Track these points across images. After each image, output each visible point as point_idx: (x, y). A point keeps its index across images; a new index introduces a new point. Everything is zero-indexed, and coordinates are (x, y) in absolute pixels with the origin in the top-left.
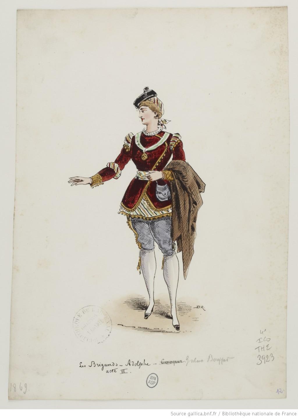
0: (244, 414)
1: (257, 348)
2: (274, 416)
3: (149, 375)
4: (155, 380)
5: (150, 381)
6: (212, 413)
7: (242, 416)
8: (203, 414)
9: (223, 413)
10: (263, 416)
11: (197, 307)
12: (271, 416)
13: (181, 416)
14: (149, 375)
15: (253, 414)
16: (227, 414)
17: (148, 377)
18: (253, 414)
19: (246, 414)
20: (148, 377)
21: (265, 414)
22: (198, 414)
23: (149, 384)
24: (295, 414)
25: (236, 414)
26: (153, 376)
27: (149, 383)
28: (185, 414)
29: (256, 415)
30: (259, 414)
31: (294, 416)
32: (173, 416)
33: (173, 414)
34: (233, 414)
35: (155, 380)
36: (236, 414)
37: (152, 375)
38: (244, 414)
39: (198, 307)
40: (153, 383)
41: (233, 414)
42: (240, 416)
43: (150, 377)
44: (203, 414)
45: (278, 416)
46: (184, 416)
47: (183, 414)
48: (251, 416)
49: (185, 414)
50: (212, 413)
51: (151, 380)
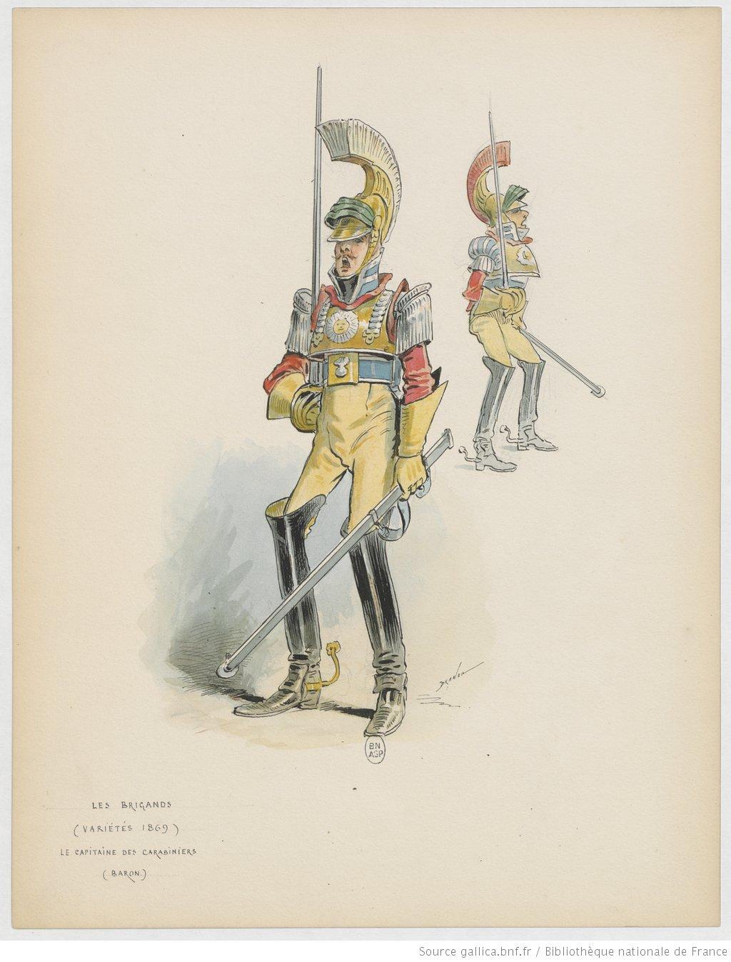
8: (498, 952)
9: (548, 949)
15: (622, 952)
16: (556, 952)
18: (622, 952)
19: (604, 953)
21: (650, 952)
25: (579, 951)
30: (635, 952)
36: (579, 951)
38: (599, 953)
47: (449, 952)
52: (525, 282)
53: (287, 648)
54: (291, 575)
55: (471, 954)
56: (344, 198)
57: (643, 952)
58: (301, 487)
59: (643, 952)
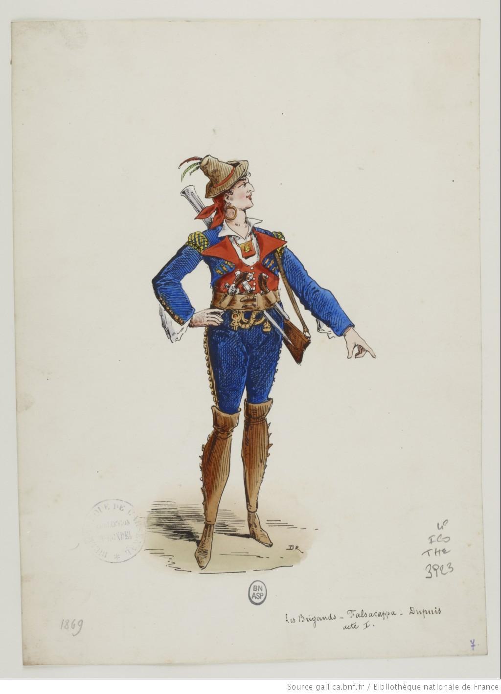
0: (411, 688)
1: (425, 552)
2: (460, 690)
3: (251, 585)
4: (262, 590)
5: (254, 594)
6: (357, 686)
7: (407, 691)
8: (342, 687)
9: (376, 685)
10: (443, 691)
11: (289, 548)
12: (455, 691)
13: (304, 691)
14: (251, 585)
15: (426, 687)
16: (381, 687)
17: (250, 588)
18: (426, 687)
19: (414, 688)
20: (250, 588)
21: (446, 687)
22: (332, 687)
23: (254, 600)
24: (496, 687)
25: (397, 687)
26: (257, 585)
27: (254, 598)
28: (311, 687)
29: (322, 688)
30: (435, 687)
31: (495, 691)
32: (292, 691)
33: (290, 687)
34: (441, 687)
35: (262, 590)
36: (397, 687)
37: (254, 584)
38: (411, 688)
39: (292, 548)
40: (259, 595)
41: (441, 687)
42: (403, 691)
43: (252, 587)
44: (342, 687)
45: (467, 691)
46: (310, 692)
47: (308, 687)
48: (422, 691)
49: (311, 687)
50: (357, 686)
51: (256, 592)
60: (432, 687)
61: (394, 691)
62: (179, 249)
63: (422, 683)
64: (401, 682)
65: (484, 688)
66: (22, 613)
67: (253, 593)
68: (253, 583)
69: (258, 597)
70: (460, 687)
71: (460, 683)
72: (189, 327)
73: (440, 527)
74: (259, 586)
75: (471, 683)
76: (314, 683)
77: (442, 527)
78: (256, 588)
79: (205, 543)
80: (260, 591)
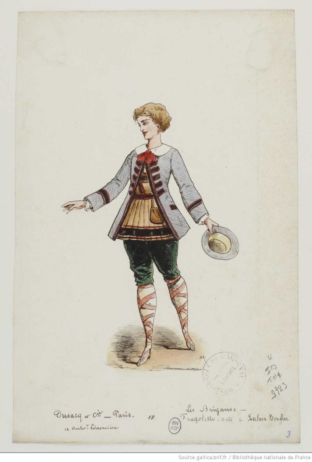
6: (222, 457)
8: (213, 457)
9: (234, 456)
13: (189, 460)
15: (265, 458)
16: (237, 458)
18: (265, 458)
19: (258, 458)
21: (277, 458)
22: (207, 458)
24: (309, 458)
25: (247, 457)
26: (175, 421)
28: (193, 458)
30: (271, 458)
31: (308, 460)
32: (182, 460)
35: (178, 424)
36: (247, 457)
37: (173, 420)
38: (256, 458)
40: (176, 428)
42: (251, 460)
43: (171, 422)
44: (213, 457)
45: (291, 460)
46: (192, 460)
47: (192, 458)
49: (193, 458)
50: (222, 457)
51: (173, 426)
52: (154, 312)
53: (169, 422)
54: (155, 172)
55: (268, 458)
56: (85, 198)
57: (244, 458)
58: (128, 199)
59: (244, 458)
60: (269, 458)
61: (246, 460)
62: (141, 153)
63: (263, 455)
64: (250, 455)
65: (302, 458)
66: (268, 10)
67: (171, 426)
68: (172, 419)
69: (174, 429)
70: (287, 458)
71: (287, 455)
72: (145, 145)
73: (270, 358)
74: (176, 422)
75: (293, 455)
76: (196, 455)
77: (271, 357)
78: (174, 423)
79: (157, 119)
80: (176, 425)
